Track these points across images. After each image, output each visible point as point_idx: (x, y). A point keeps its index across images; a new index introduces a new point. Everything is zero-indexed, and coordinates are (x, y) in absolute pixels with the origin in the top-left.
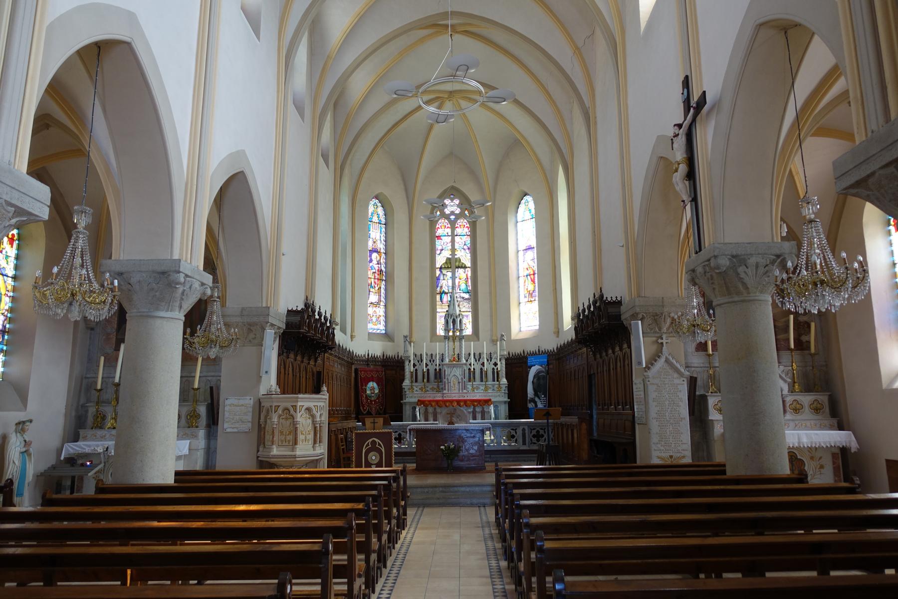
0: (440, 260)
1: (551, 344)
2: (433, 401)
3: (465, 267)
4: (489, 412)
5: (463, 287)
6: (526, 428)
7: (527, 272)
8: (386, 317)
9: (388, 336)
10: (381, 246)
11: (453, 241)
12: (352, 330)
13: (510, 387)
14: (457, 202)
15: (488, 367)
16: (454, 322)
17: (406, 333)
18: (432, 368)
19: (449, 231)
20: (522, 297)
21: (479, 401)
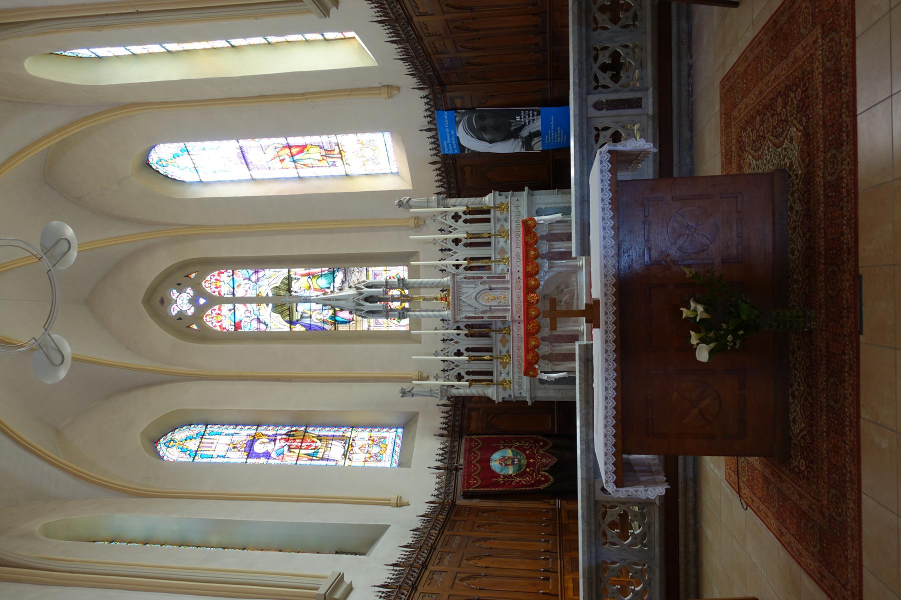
0: (277, 324)
1: (413, 102)
2: (527, 343)
3: (289, 279)
4: (551, 224)
5: (323, 282)
6: (593, 99)
7: (288, 162)
8: (373, 426)
9: (408, 424)
10: (244, 434)
11: (242, 301)
12: (386, 503)
13: (503, 188)
14: (174, 294)
15: (462, 231)
16: (370, 299)
17: (394, 389)
18: (466, 343)
19: (226, 307)
20: (334, 171)
21: (527, 246)
